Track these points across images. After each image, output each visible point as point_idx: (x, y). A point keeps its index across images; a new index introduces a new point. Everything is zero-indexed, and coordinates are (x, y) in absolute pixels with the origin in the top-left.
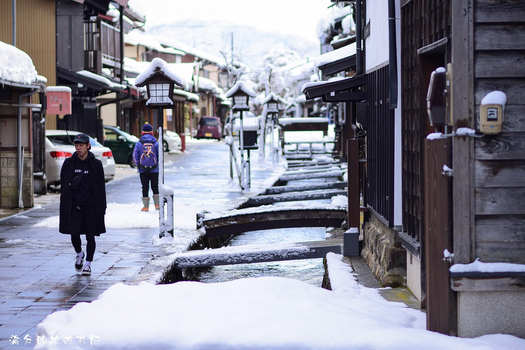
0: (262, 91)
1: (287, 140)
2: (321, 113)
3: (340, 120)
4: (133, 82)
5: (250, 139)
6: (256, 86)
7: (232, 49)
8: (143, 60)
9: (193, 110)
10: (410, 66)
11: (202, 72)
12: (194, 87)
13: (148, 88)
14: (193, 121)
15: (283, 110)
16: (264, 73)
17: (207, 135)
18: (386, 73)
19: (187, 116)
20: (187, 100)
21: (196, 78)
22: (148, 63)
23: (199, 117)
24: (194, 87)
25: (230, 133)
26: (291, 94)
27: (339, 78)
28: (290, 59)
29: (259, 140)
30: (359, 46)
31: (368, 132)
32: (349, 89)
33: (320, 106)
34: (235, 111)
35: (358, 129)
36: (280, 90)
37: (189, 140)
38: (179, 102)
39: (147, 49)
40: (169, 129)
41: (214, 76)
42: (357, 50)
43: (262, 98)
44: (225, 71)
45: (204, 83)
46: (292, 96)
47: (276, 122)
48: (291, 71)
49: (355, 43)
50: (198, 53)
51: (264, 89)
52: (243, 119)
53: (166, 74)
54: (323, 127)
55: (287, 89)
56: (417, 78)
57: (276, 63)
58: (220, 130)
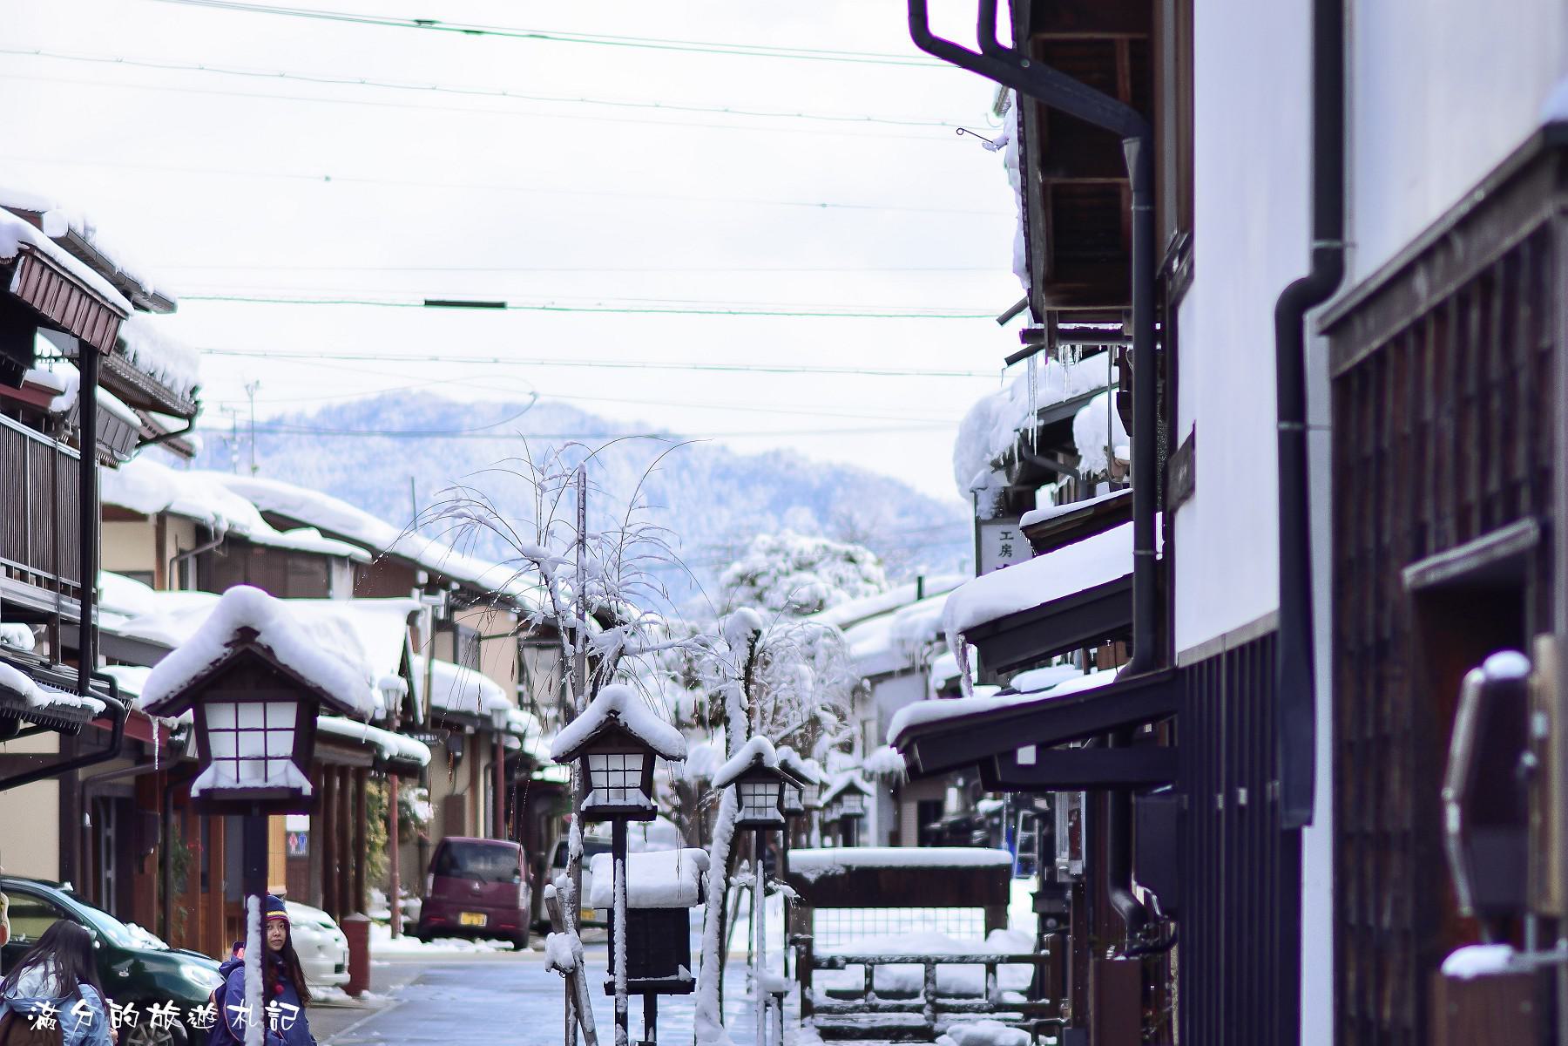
0: (715, 723)
1: (823, 948)
2: (980, 825)
3: (1062, 859)
4: (138, 684)
5: (656, 948)
6: (688, 699)
7: (581, 542)
8: (183, 586)
9: (405, 805)
10: (1370, 639)
11: (446, 637)
12: (408, 702)
13: (200, 719)
14: (405, 857)
15: (809, 809)
16: (721, 647)
17: (465, 919)
18: (1265, 662)
19: (378, 834)
20: (379, 763)
21: (418, 662)
22: (210, 601)
23: (433, 839)
24: (408, 702)
25: (568, 917)
26: (843, 736)
27: (1064, 678)
28: (841, 581)
29: (700, 941)
30: (1144, 539)
31: (1181, 927)
32: (1100, 734)
33: (971, 796)
34: (593, 816)
35: (1141, 913)
36: (795, 721)
37: (381, 940)
38: (343, 771)
39: (201, 532)
40: (293, 896)
41: (500, 653)
42: (1137, 559)
43: (711, 757)
44: (548, 633)
45: (455, 684)
46: (847, 747)
47: (776, 869)
48: (845, 636)
49: (1129, 527)
50: (433, 552)
51: (720, 719)
52: (630, 856)
53: (282, 657)
54: (986, 891)
55: (829, 719)
56: (1401, 697)
57: (776, 597)
58: (524, 901)
